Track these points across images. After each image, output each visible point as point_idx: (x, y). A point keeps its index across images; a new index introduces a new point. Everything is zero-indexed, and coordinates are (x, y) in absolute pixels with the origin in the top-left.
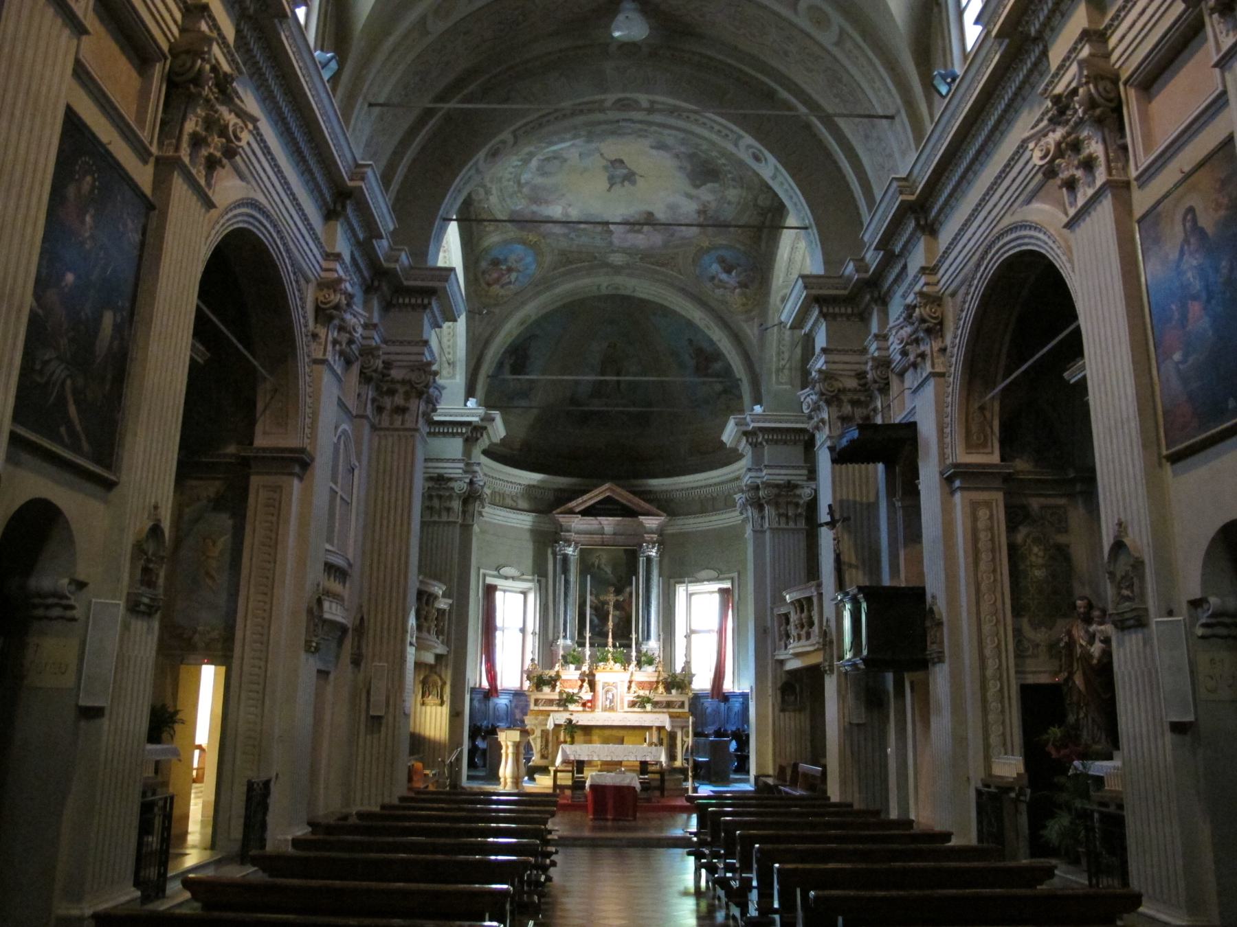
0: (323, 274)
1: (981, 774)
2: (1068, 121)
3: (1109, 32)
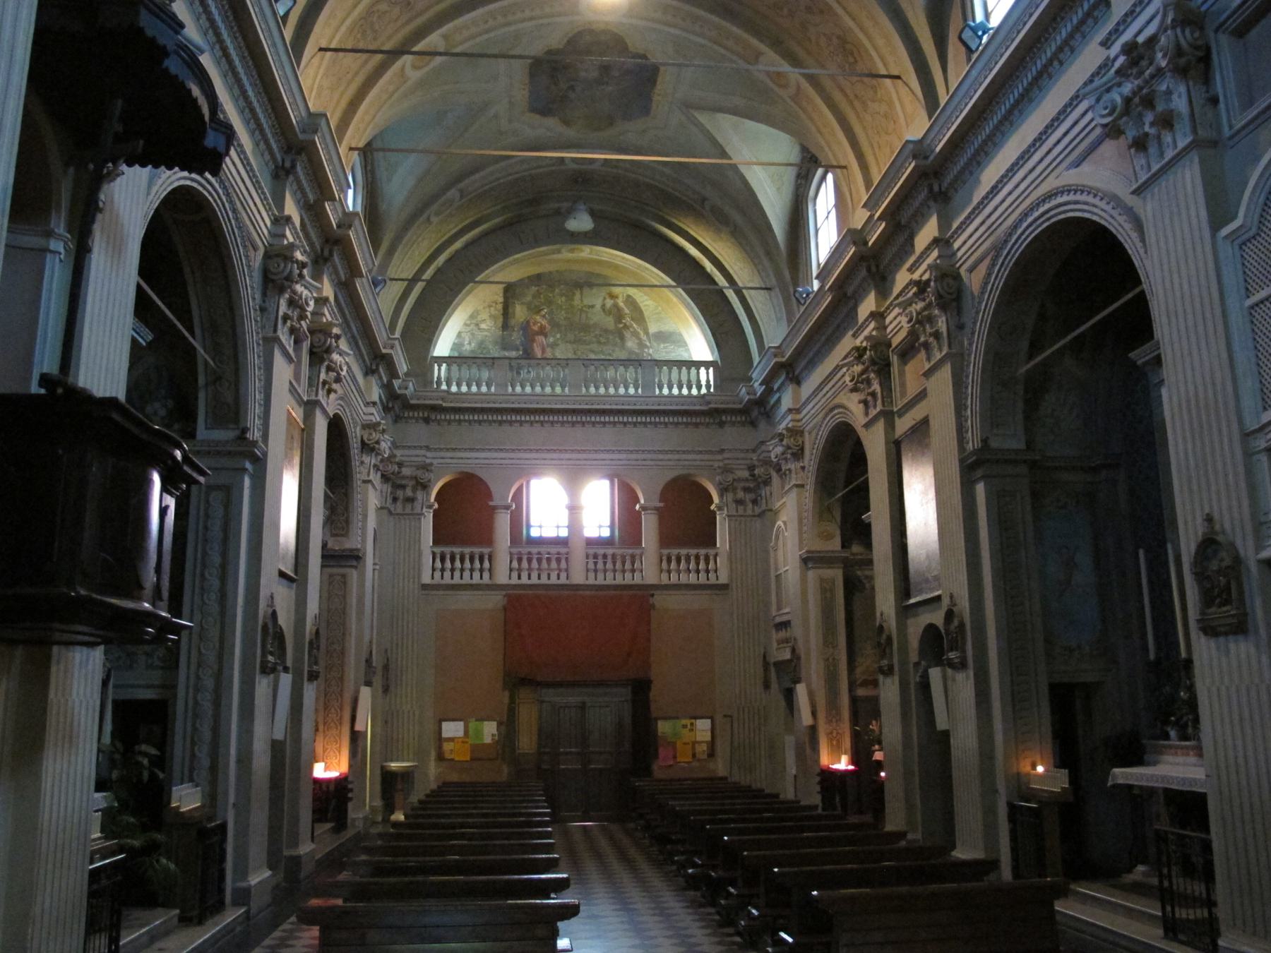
0: (365, 417)
2: (1141, 73)
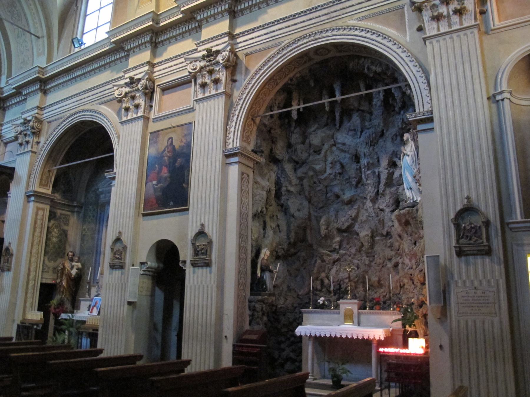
1: (21, 318)
2: (133, 87)
3: (156, 66)
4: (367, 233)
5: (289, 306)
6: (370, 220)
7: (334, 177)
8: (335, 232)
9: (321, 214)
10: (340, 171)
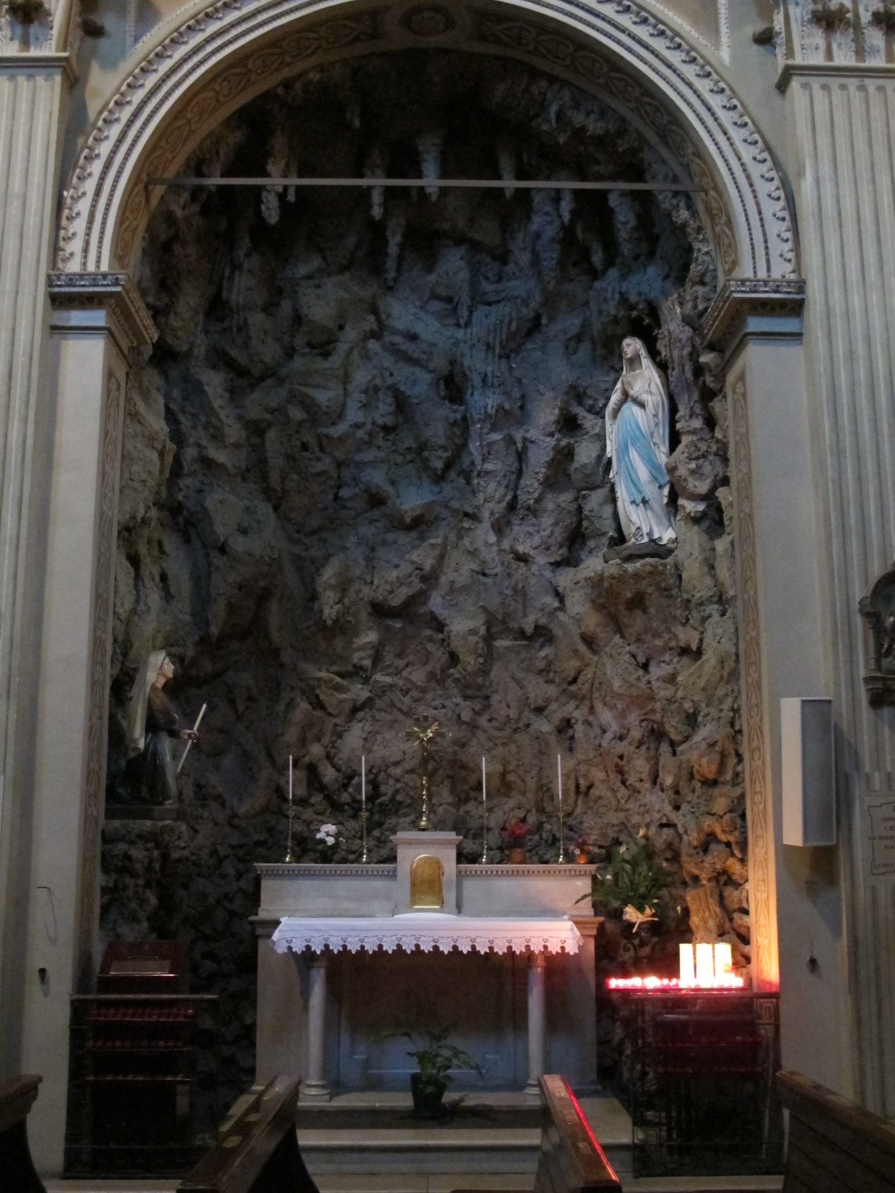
4: (470, 624)
5: (205, 854)
6: (485, 584)
7: (366, 438)
8: (364, 616)
9: (315, 552)
10: (389, 421)
